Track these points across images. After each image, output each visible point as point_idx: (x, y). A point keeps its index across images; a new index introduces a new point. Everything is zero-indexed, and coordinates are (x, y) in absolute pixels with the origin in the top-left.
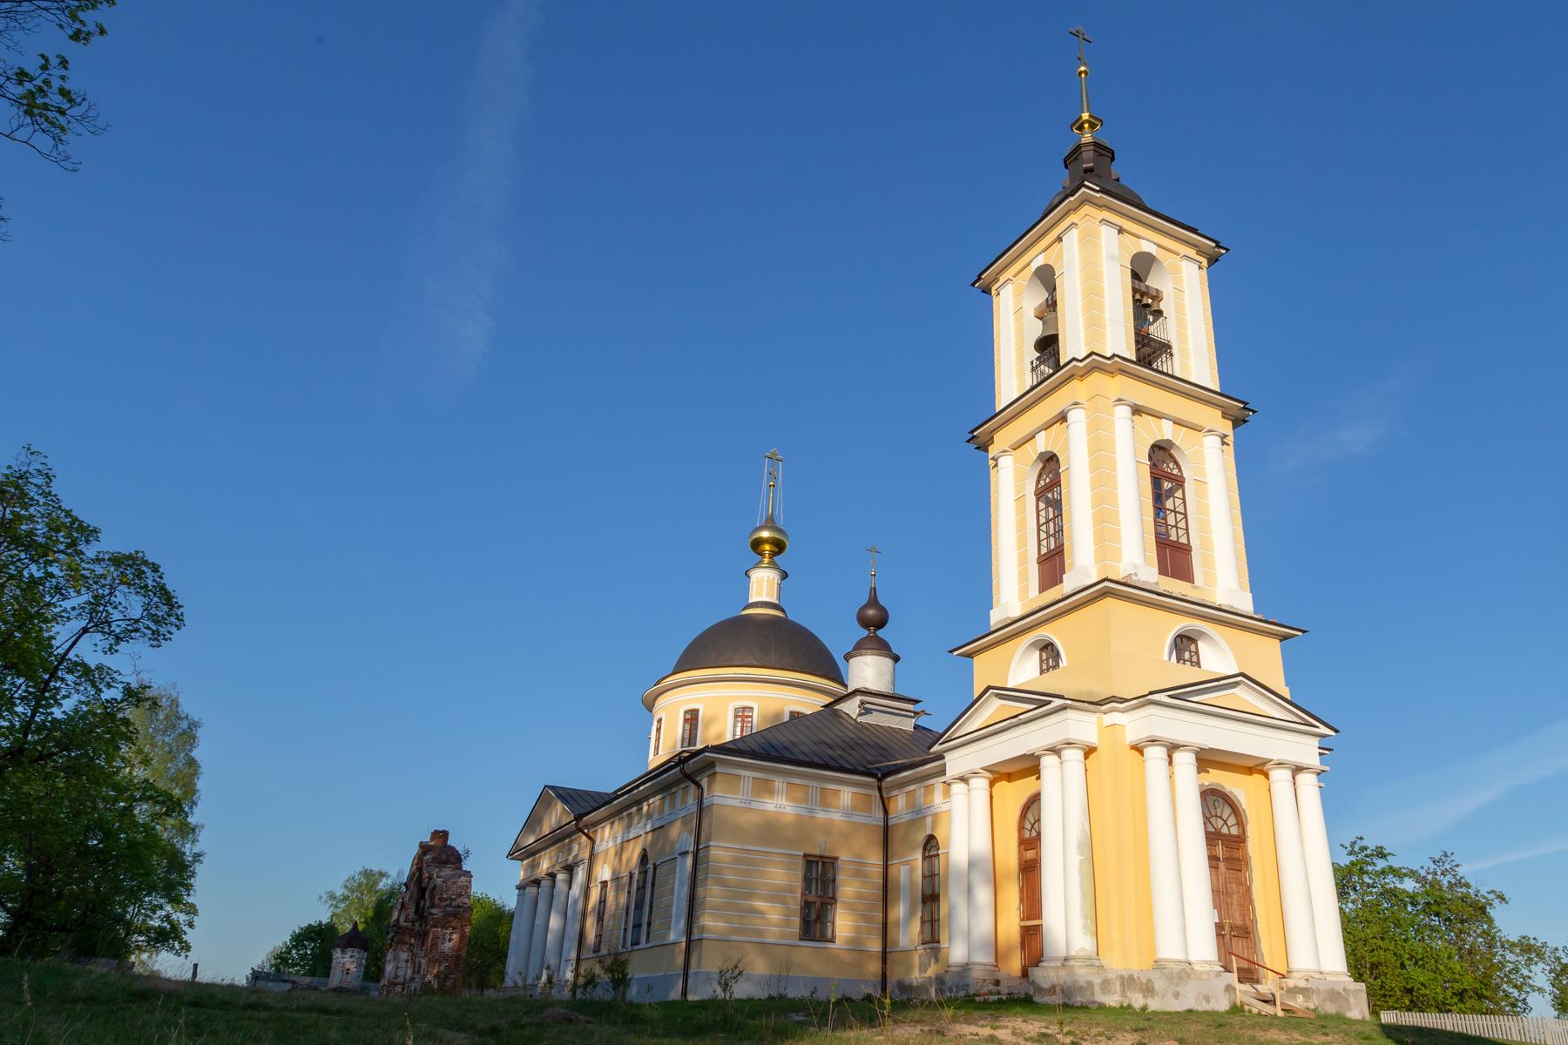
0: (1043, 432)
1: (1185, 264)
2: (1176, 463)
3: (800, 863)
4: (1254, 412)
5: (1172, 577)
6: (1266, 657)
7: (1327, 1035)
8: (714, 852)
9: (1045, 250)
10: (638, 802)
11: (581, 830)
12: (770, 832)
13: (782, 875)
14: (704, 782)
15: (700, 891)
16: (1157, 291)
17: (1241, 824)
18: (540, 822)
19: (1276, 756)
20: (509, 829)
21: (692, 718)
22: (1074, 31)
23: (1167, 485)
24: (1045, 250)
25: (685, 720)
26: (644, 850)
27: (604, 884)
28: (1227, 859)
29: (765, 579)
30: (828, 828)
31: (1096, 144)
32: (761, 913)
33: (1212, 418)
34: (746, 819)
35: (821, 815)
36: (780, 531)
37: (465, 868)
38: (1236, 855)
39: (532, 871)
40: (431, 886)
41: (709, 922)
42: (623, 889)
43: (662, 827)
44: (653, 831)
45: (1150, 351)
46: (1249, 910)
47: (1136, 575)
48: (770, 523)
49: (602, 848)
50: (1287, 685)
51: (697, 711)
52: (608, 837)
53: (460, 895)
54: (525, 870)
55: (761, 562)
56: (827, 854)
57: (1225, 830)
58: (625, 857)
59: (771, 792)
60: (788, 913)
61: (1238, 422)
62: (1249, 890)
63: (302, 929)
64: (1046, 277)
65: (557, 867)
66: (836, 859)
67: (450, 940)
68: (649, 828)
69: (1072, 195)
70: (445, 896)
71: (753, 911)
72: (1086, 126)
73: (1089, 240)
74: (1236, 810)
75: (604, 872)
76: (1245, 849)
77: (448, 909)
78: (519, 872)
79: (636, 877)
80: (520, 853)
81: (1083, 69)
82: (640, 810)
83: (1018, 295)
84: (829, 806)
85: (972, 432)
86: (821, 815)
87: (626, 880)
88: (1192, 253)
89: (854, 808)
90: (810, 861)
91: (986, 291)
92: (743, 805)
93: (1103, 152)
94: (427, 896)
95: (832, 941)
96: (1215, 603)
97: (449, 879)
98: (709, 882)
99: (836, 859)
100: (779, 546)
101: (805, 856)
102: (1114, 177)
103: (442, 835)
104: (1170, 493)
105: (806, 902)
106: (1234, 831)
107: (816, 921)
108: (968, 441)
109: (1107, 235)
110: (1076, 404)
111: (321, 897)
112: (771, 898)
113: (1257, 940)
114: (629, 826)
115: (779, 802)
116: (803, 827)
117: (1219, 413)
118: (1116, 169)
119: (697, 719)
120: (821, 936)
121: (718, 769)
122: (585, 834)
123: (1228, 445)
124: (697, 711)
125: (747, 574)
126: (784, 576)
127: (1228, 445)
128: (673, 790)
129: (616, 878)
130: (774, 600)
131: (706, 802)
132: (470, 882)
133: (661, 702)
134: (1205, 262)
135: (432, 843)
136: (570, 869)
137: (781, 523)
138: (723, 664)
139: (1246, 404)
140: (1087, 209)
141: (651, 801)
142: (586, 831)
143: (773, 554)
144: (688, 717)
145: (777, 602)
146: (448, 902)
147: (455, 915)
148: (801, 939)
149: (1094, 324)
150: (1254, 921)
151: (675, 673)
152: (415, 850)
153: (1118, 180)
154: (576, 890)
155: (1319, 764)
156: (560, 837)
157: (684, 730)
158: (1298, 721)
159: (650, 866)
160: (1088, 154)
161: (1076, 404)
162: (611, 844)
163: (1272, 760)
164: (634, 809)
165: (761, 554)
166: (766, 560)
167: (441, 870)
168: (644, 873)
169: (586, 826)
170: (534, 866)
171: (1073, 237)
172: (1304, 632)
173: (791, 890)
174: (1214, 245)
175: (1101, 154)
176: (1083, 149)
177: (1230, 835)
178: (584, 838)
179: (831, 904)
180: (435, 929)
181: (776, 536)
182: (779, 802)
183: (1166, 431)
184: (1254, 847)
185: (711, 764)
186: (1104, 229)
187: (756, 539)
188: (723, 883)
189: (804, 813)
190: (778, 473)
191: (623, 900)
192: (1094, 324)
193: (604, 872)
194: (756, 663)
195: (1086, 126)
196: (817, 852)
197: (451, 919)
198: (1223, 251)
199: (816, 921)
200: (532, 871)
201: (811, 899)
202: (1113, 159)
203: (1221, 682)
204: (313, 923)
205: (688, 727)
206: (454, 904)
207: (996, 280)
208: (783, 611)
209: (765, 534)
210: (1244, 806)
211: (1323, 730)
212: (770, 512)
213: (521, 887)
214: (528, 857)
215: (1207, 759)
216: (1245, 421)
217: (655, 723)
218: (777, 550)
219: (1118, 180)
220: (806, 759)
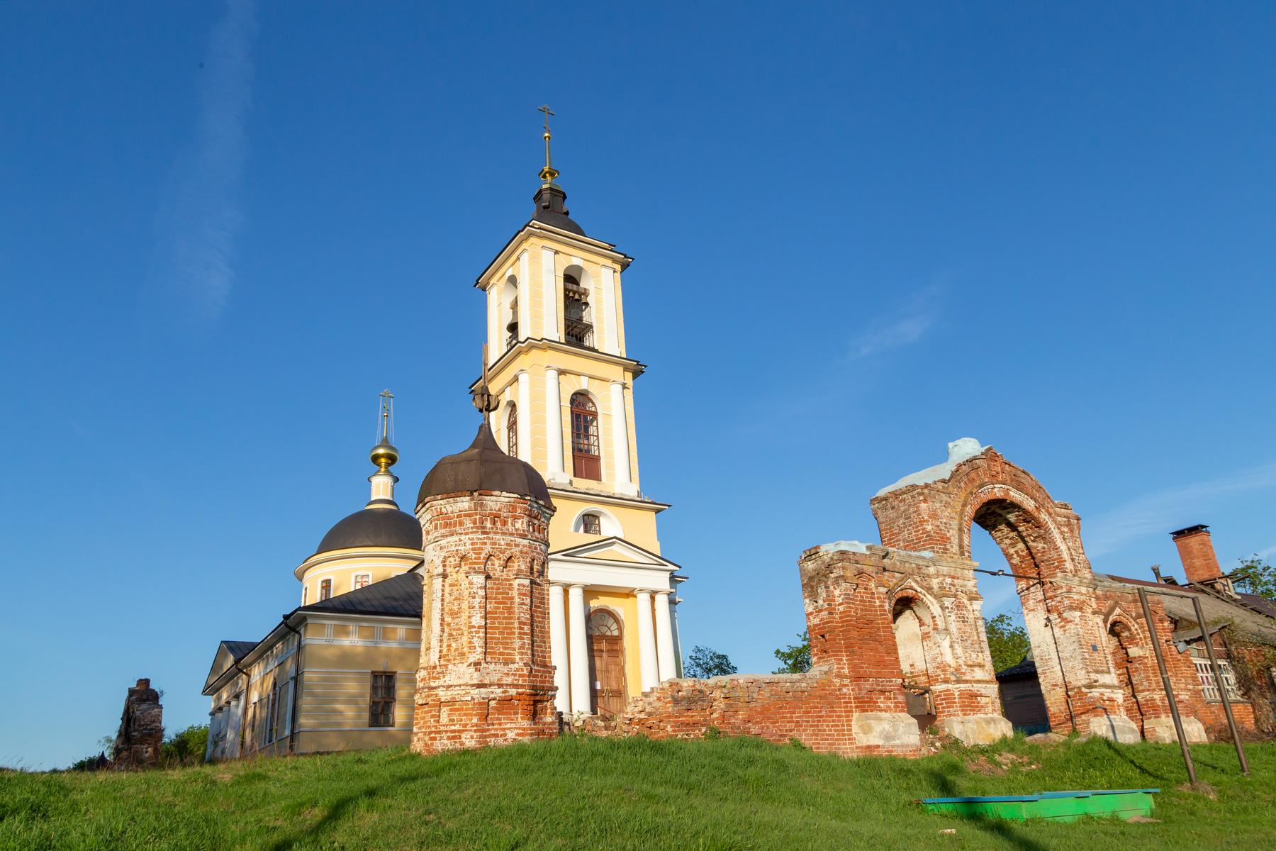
0: (509, 388)
1: (604, 270)
2: (593, 403)
3: (369, 677)
4: (645, 366)
5: (586, 478)
6: (644, 527)
7: (454, 725)
8: (306, 676)
9: (513, 265)
10: (271, 647)
11: (241, 671)
12: (346, 659)
13: (355, 687)
14: (302, 632)
15: (300, 702)
16: (585, 289)
17: (620, 629)
18: (221, 667)
19: (638, 585)
20: (202, 675)
21: (327, 585)
22: (542, 108)
23: (590, 418)
24: (513, 265)
25: (323, 587)
26: (275, 678)
27: (255, 703)
28: (608, 651)
29: (382, 483)
30: (388, 655)
31: (551, 189)
32: (340, 713)
33: (616, 372)
34: (329, 653)
35: (383, 646)
36: (392, 448)
37: (160, 703)
38: (615, 648)
39: (218, 702)
40: (134, 717)
41: (305, 721)
42: (264, 707)
43: (283, 662)
44: (278, 665)
45: (576, 333)
46: (622, 680)
47: (554, 479)
48: (385, 443)
49: (254, 681)
50: (658, 540)
51: (330, 580)
52: (257, 672)
53: (154, 722)
54: (215, 702)
55: (379, 471)
56: (388, 670)
57: (609, 633)
58: (265, 685)
59: (347, 634)
60: (360, 710)
61: (636, 374)
62: (623, 668)
63: (75, 765)
64: (513, 280)
65: (231, 697)
66: (395, 673)
67: (146, 752)
68: (276, 664)
69: (522, 231)
70: (142, 723)
71: (335, 711)
72: (547, 175)
73: (535, 260)
74: (617, 620)
75: (254, 697)
76: (622, 643)
77: (144, 731)
78: (210, 703)
79: (271, 697)
80: (211, 689)
81: (547, 135)
82: (272, 652)
83: (499, 294)
84: (389, 639)
85: (471, 387)
86: (383, 646)
87: (265, 700)
88: (608, 262)
89: (406, 639)
90: (375, 675)
91: (484, 290)
92: (326, 643)
93: (556, 193)
94: (132, 725)
95: (393, 726)
96: (610, 493)
97: (146, 711)
98: (303, 695)
99: (395, 673)
100: (392, 459)
101: (372, 672)
102: (565, 211)
103: (145, 683)
104: (592, 421)
105: (373, 702)
106: (616, 633)
107: (381, 714)
108: (470, 393)
109: (547, 256)
110: (522, 370)
111: (100, 742)
112: (348, 702)
113: (627, 697)
114: (267, 664)
115: (354, 639)
116: (369, 654)
117: (621, 369)
118: (567, 206)
119: (330, 586)
120: (384, 723)
121: (309, 621)
122: (244, 673)
123: (629, 388)
124: (330, 580)
125: (369, 480)
126: (396, 480)
127: (629, 388)
128: (288, 637)
129: (260, 700)
130: (389, 498)
131: (303, 643)
132: (161, 712)
133: (308, 575)
134: (618, 268)
135: (137, 688)
136: (237, 697)
137: (393, 443)
138: (357, 545)
139: (638, 362)
140: (532, 240)
141: (277, 646)
142: (245, 671)
143: (388, 465)
144: (324, 585)
145: (391, 499)
146: (145, 727)
147: (150, 735)
148: (370, 726)
149: (536, 317)
150: (625, 687)
151: (319, 552)
152: (126, 694)
153: (567, 213)
154: (240, 711)
155: (669, 587)
156: (230, 677)
157: (322, 594)
158: (656, 563)
159: (277, 688)
160: (546, 196)
161: (522, 370)
162: (258, 677)
163: (636, 589)
164: (269, 652)
165: (379, 465)
166: (383, 469)
167: (140, 706)
168: (274, 694)
169: (245, 667)
170: (219, 698)
171: (525, 257)
172: (669, 506)
173: (362, 695)
174: (623, 256)
175: (556, 196)
176: (543, 192)
177: (612, 636)
178: (244, 676)
179: (391, 702)
180: (135, 746)
181: (389, 452)
182: (354, 639)
183: (583, 384)
184: (627, 642)
185: (304, 618)
186: (544, 252)
187: (374, 455)
188: (313, 695)
189: (369, 644)
190: (390, 406)
191: (264, 714)
192: (536, 317)
193: (254, 697)
194: (371, 544)
195: (547, 175)
196: (381, 669)
197: (147, 738)
198: (631, 260)
199: (381, 714)
200: (218, 702)
201: (377, 700)
202: (565, 197)
203: (600, 544)
204: (84, 760)
205: (324, 592)
206: (148, 728)
207: (488, 283)
208: (395, 504)
209: (381, 451)
210: (622, 618)
211: (671, 567)
212: (385, 435)
213: (212, 714)
214: (215, 693)
215: (590, 592)
216: (643, 372)
217: (304, 591)
218: (390, 462)
219: (567, 213)
220: (374, 610)
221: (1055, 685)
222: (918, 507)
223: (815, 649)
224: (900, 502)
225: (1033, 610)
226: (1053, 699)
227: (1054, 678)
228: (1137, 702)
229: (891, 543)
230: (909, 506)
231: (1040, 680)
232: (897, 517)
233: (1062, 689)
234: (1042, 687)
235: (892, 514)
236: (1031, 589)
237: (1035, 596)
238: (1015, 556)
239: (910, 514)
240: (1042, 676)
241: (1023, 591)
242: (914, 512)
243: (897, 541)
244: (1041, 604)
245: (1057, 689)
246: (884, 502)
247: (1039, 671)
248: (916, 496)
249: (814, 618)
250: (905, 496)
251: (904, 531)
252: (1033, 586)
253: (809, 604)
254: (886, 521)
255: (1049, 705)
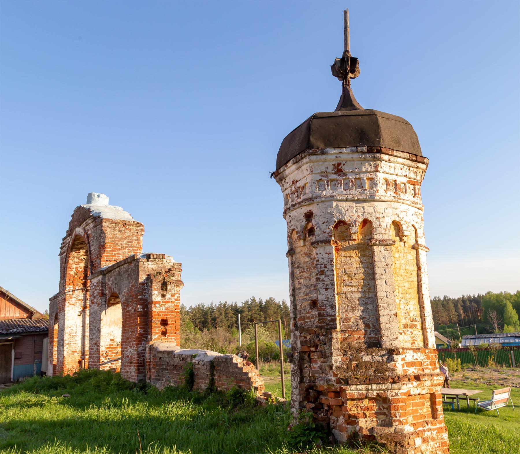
221: (74, 352)
222: (139, 238)
223: (157, 329)
224: (127, 229)
225: (73, 305)
226: (70, 360)
227: (75, 347)
228: (395, 389)
229: (113, 254)
230: (133, 234)
231: (65, 348)
232: (122, 238)
233: (79, 354)
234: (65, 353)
235: (119, 235)
236: (76, 291)
237: (78, 296)
238: (74, 270)
239: (133, 240)
240: (67, 345)
241: (70, 292)
242: (136, 240)
243: (118, 254)
244: (80, 302)
245: (76, 354)
246: (114, 225)
247: (66, 342)
248: (140, 230)
249: (161, 306)
250: (131, 227)
251: (125, 249)
252: (77, 290)
253: (158, 295)
254: (113, 238)
255: (66, 364)
